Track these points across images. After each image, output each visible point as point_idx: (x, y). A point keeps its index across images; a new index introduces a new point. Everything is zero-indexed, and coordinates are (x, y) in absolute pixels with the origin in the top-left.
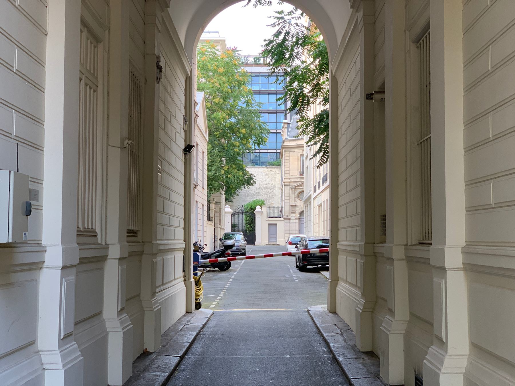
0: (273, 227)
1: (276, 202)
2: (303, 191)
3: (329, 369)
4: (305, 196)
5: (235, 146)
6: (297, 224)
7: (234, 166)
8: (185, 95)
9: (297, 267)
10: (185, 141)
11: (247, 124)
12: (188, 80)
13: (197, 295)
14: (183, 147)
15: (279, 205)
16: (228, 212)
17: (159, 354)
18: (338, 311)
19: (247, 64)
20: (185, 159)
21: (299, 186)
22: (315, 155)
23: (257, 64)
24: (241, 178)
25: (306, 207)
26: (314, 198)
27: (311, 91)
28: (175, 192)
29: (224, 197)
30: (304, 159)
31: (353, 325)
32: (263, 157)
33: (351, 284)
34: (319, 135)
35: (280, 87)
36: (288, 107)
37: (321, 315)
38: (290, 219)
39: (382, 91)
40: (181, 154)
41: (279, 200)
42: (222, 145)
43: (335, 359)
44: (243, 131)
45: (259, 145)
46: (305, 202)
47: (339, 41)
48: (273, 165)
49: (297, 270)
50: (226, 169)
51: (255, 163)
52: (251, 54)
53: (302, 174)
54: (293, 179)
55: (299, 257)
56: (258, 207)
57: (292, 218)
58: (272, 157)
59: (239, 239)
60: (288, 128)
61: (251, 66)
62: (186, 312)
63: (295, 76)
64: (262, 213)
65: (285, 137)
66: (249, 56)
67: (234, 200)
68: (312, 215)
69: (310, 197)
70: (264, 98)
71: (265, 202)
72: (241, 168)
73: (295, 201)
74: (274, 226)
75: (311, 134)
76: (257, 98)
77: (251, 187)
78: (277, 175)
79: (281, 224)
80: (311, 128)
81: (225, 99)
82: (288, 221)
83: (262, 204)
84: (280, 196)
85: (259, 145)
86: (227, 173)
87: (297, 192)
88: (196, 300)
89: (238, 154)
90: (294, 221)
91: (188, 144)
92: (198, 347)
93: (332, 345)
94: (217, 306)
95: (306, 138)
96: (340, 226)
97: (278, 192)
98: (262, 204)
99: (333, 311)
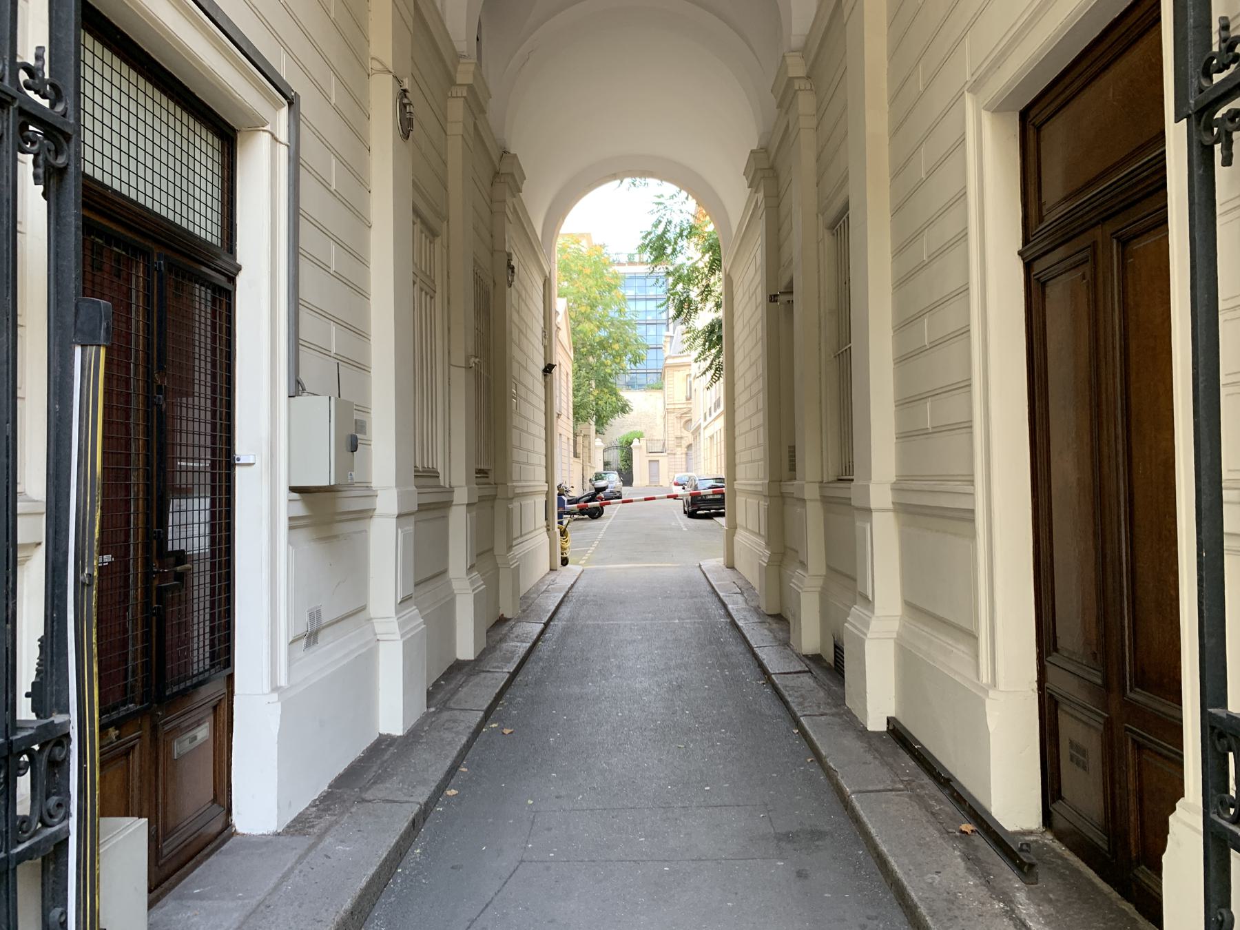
1: (658, 434)
2: (691, 420)
3: (727, 635)
4: (693, 426)
6: (684, 460)
7: (606, 391)
10: (545, 359)
12: (547, 283)
15: (662, 438)
16: (600, 447)
17: (519, 620)
20: (545, 382)
24: (614, 404)
25: (695, 438)
26: (705, 428)
28: (534, 422)
29: (593, 428)
32: (642, 379)
38: (674, 454)
46: (692, 433)
48: (653, 388)
49: (685, 517)
50: (595, 393)
51: (631, 386)
53: (689, 398)
58: (652, 378)
60: (671, 343)
62: (551, 570)
63: (680, 277)
64: (640, 448)
65: (666, 354)
67: (606, 432)
71: (645, 435)
72: (614, 393)
73: (681, 432)
75: (700, 349)
79: (663, 460)
80: (700, 341)
81: (593, 306)
82: (673, 456)
84: (662, 426)
86: (597, 399)
87: (683, 421)
90: (680, 456)
91: (548, 362)
92: (565, 612)
93: (730, 607)
95: (695, 354)
97: (660, 421)
99: (731, 566)
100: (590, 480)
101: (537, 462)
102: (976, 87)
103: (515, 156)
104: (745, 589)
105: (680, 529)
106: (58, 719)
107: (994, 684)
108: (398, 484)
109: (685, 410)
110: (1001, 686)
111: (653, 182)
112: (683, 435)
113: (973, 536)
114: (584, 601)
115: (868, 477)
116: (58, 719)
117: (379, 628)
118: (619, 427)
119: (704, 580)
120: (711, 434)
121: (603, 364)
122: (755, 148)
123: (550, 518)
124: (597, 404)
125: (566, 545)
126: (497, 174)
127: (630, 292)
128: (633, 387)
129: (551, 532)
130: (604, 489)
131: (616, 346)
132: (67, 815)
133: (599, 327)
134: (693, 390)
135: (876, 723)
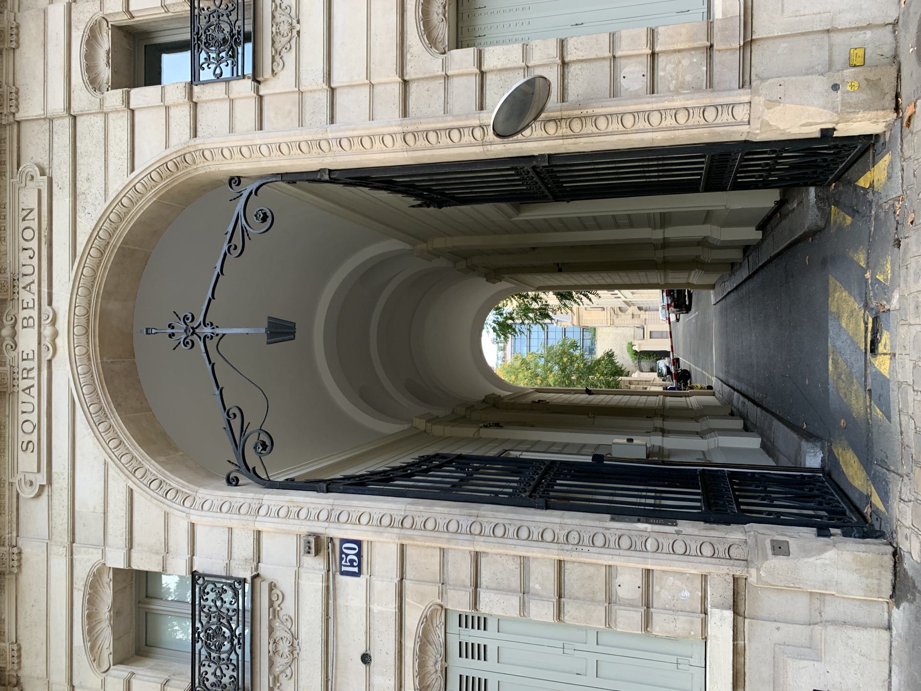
0: (654, 335)
1: (629, 332)
2: (619, 308)
3: (744, 290)
4: (624, 306)
5: (579, 367)
6: (650, 312)
7: (597, 368)
8: (549, 393)
9: (687, 313)
10: (582, 394)
11: (559, 356)
12: (538, 391)
13: (701, 388)
14: (587, 395)
15: (632, 329)
16: (639, 375)
17: (732, 405)
18: (713, 283)
19: (504, 357)
20: (596, 394)
21: (614, 312)
22: (590, 300)
23: (504, 348)
24: (607, 362)
25: (634, 305)
26: (626, 298)
27: (537, 303)
28: (621, 400)
29: (624, 378)
30: (589, 307)
31: (719, 276)
32: (588, 343)
33: (689, 275)
34: (573, 297)
35: (536, 328)
36: (549, 321)
37: (716, 296)
38: (645, 320)
39: (558, 264)
40: (592, 397)
41: (627, 329)
42: (578, 378)
43: (736, 288)
44: (565, 360)
45: (578, 347)
46: (630, 306)
47: (513, 286)
48: (595, 335)
49: (690, 313)
50: (599, 375)
51: (592, 351)
52: (496, 353)
53: (603, 309)
54: (125, 135)
55: (678, 311)
56: (634, 348)
57: (645, 317)
58: (588, 335)
59: (662, 364)
60: (562, 321)
61: (505, 354)
62: (714, 395)
63: (525, 315)
64: (640, 345)
65: (570, 325)
66: (498, 355)
67: (626, 370)
68: (641, 299)
69: (625, 302)
70: (534, 342)
71: (630, 342)
72: (598, 362)
73: (629, 314)
74: (652, 333)
75: (573, 303)
76: (533, 350)
77: (615, 354)
78: (604, 330)
79: (649, 328)
80: (567, 302)
81: (537, 375)
82: (647, 321)
83: (631, 345)
84: (624, 328)
85: (578, 347)
86: (602, 374)
87: (620, 313)
88: (705, 389)
89: (585, 364)
90: (647, 316)
91: (585, 392)
92: (732, 382)
93: (729, 290)
94: (712, 375)
95: (575, 306)
96: (647, 283)
97: (620, 330)
98: (631, 345)
99: (713, 287)
100: (663, 380)
101: (645, 400)
102: (510, 217)
103: (486, 396)
104: (722, 281)
105: (696, 317)
106: (698, 473)
107: (725, 206)
108: (650, 436)
109: (612, 311)
110: (725, 204)
111: (483, 333)
112: (631, 313)
113: (670, 213)
114: (727, 373)
115: (650, 239)
116: (698, 473)
117: (712, 446)
118: (624, 359)
119: (720, 303)
120: (631, 294)
121: (577, 369)
122: (485, 279)
123: (681, 395)
124: (606, 374)
125: (699, 386)
126: (494, 406)
127: (525, 350)
128: (593, 350)
129: (690, 395)
130: (668, 368)
131: (565, 360)
132: (723, 471)
133: (551, 372)
134: (598, 306)
135: (758, 235)
